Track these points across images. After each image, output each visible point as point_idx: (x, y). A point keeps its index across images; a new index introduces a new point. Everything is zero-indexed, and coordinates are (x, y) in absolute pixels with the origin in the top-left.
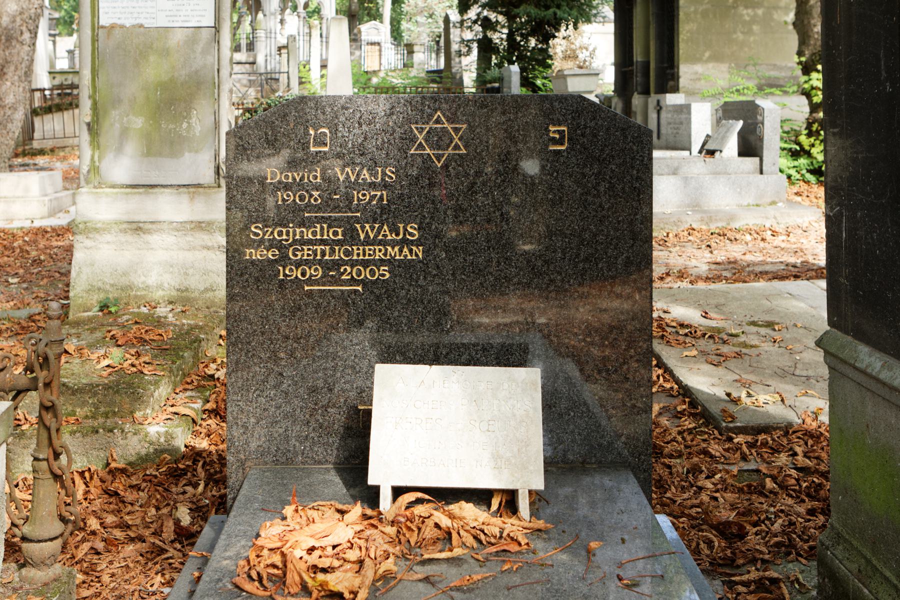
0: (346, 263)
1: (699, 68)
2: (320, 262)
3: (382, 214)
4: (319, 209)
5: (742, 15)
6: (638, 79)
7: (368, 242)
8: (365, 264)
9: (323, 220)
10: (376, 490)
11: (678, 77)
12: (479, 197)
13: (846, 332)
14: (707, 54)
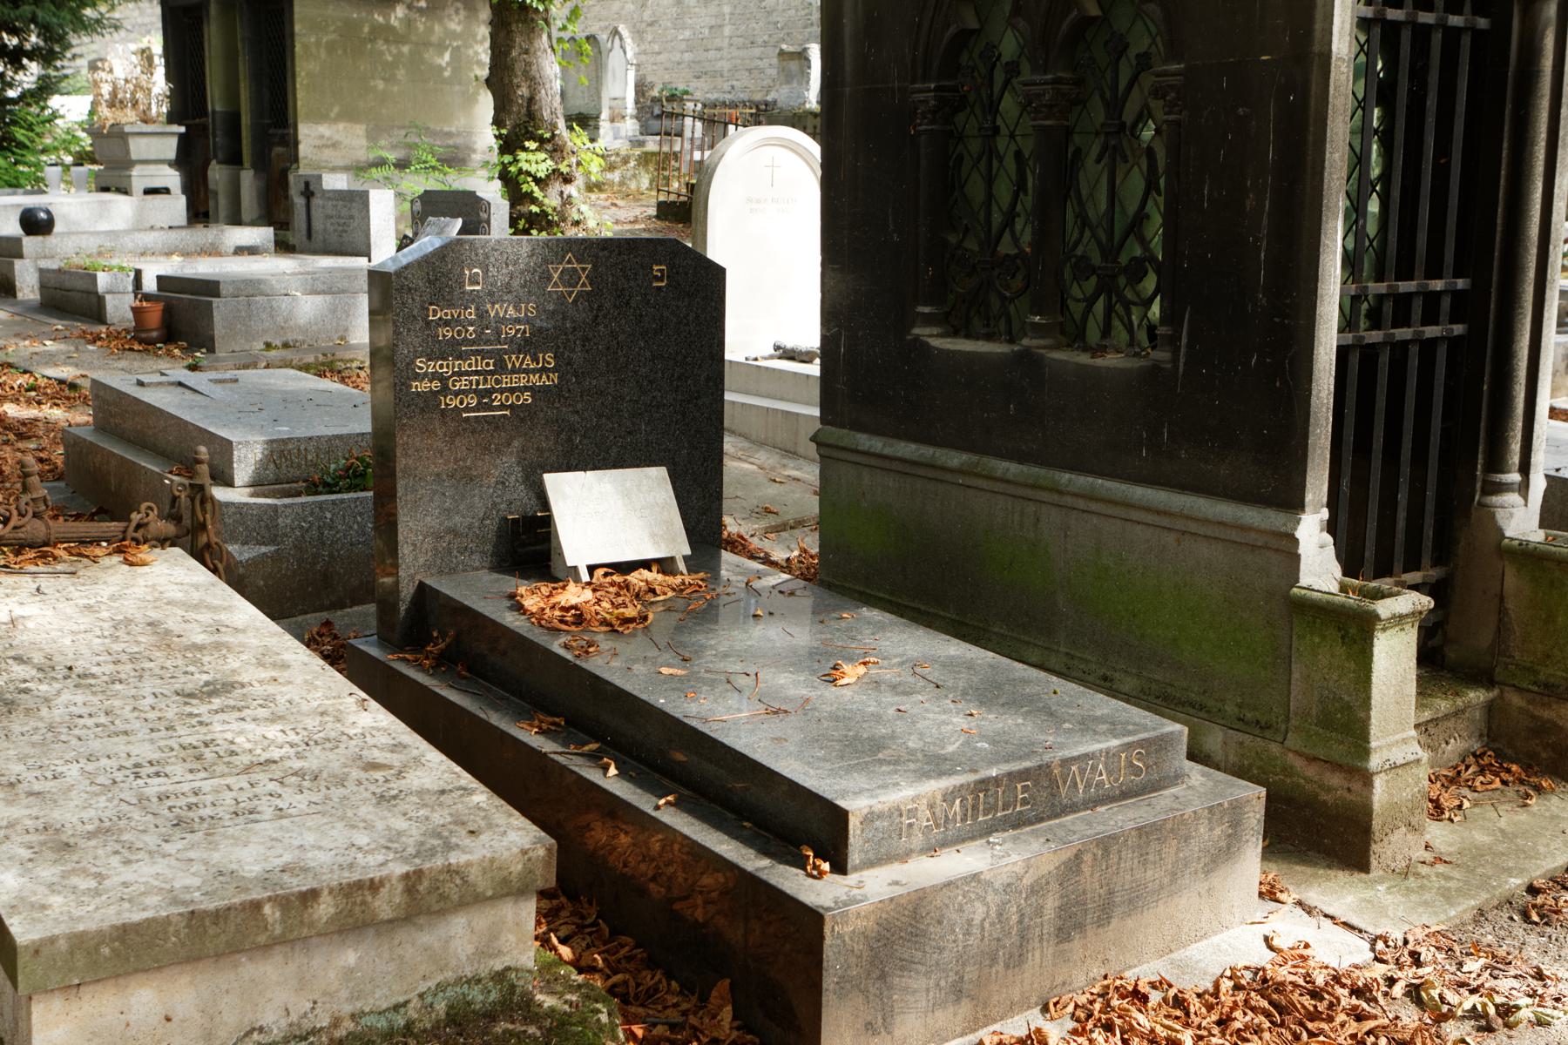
0: (495, 391)
1: (324, 130)
2: (475, 391)
3: (528, 345)
4: (473, 343)
5: (381, 53)
6: (219, 139)
7: (514, 371)
8: (512, 390)
9: (477, 352)
10: (575, 568)
11: (296, 143)
12: (601, 328)
13: (842, 426)
14: (336, 109)
